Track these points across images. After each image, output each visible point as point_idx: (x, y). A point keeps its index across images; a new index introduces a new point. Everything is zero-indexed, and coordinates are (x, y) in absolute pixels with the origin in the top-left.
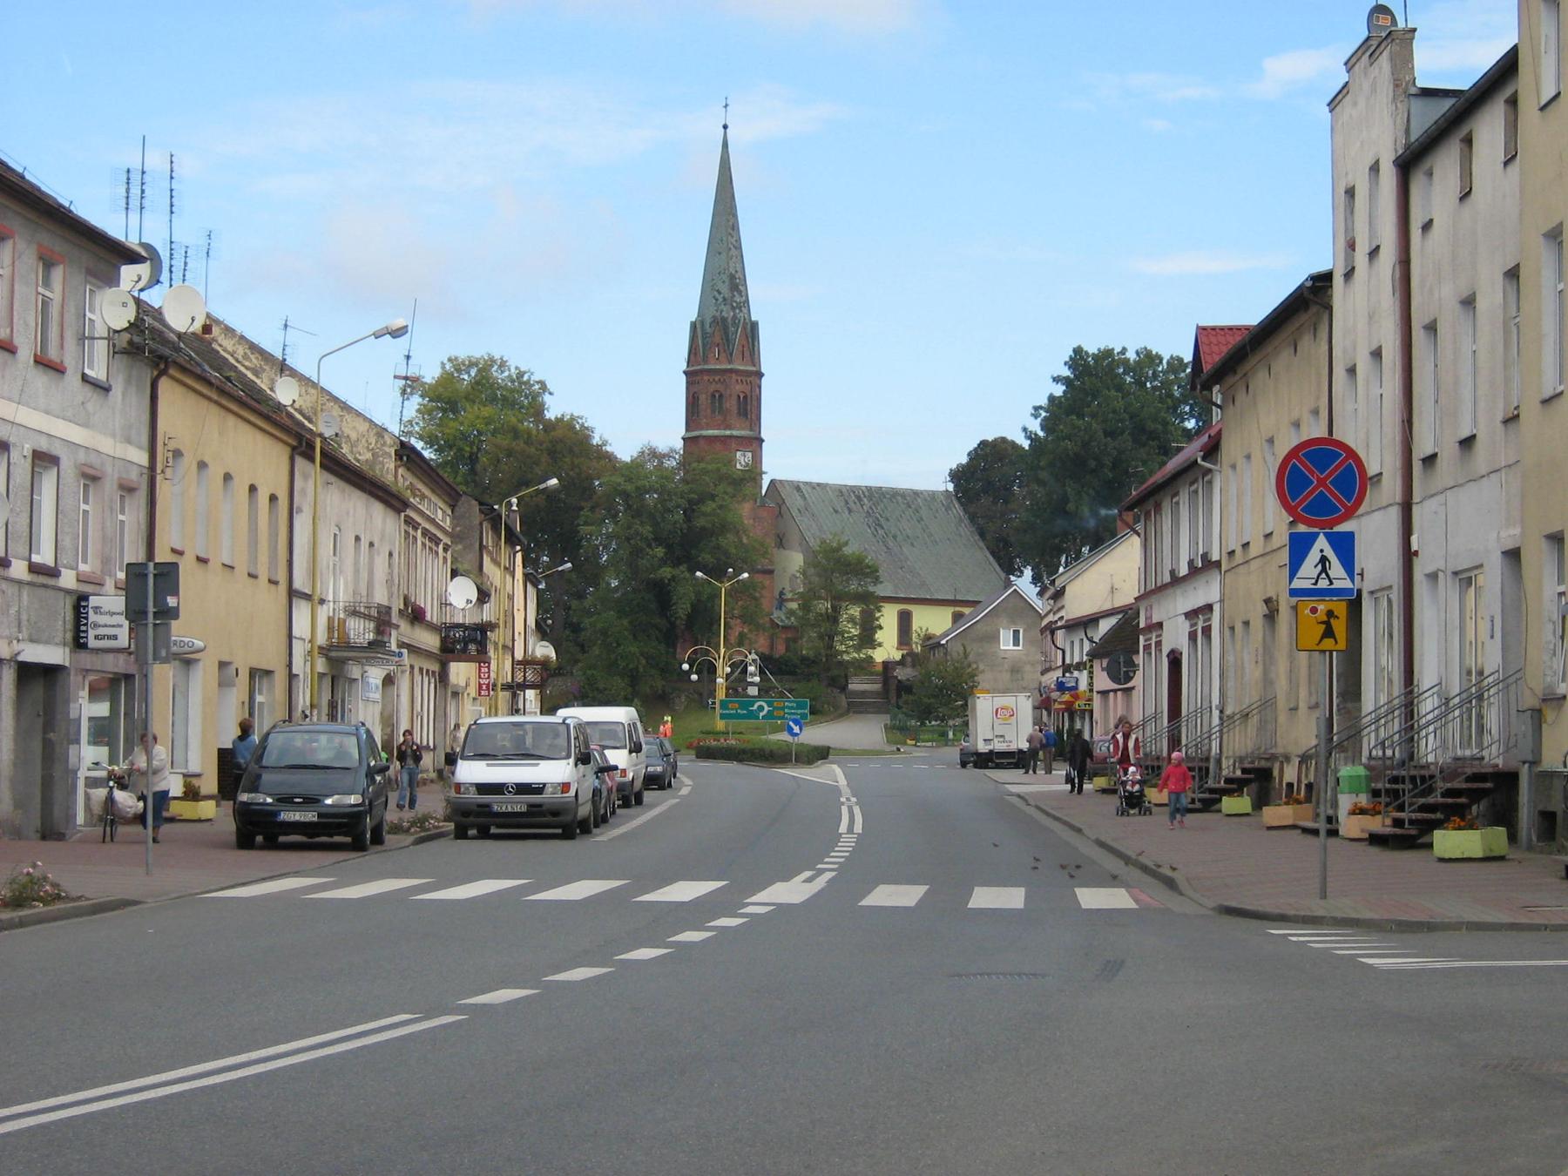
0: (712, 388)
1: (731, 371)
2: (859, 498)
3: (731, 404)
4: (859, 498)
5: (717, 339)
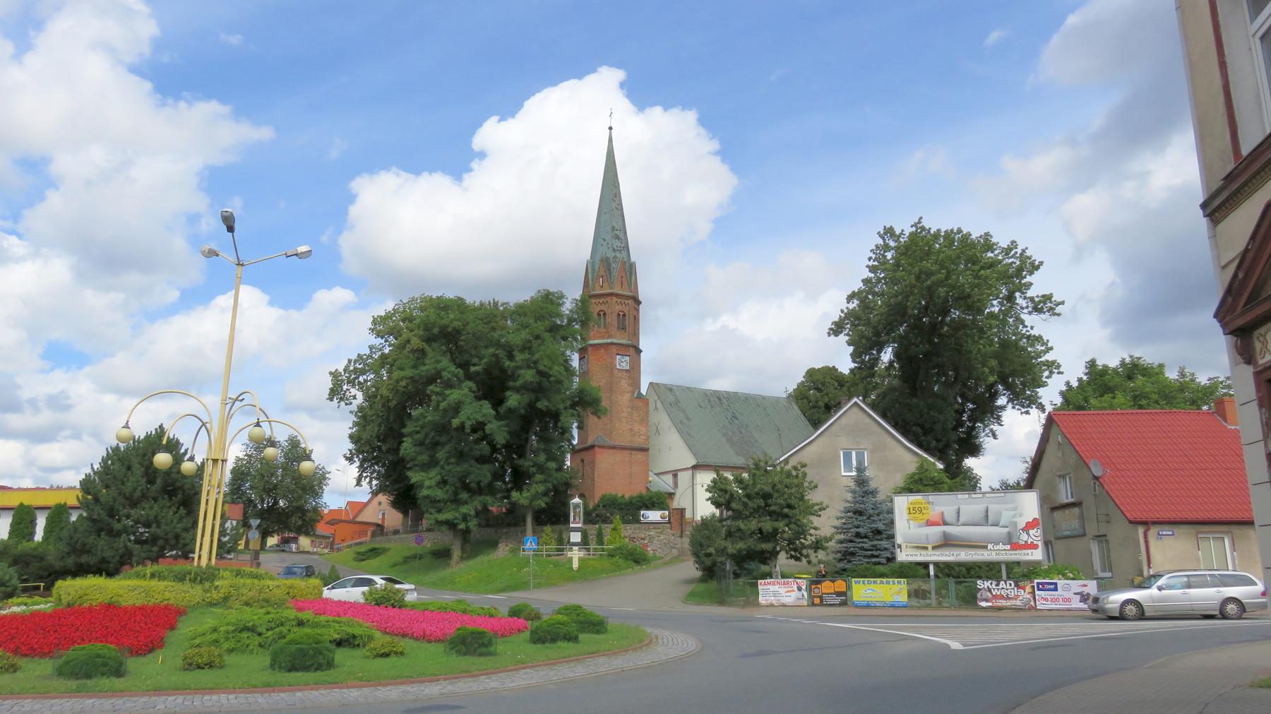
0: (598, 309)
1: (611, 294)
2: (719, 399)
3: (612, 320)
4: (719, 399)
5: (602, 273)
